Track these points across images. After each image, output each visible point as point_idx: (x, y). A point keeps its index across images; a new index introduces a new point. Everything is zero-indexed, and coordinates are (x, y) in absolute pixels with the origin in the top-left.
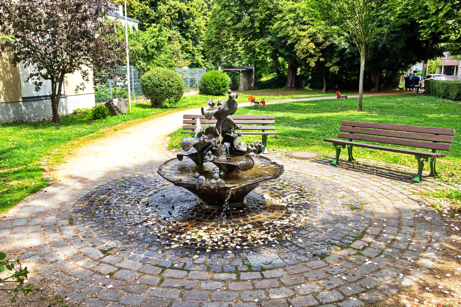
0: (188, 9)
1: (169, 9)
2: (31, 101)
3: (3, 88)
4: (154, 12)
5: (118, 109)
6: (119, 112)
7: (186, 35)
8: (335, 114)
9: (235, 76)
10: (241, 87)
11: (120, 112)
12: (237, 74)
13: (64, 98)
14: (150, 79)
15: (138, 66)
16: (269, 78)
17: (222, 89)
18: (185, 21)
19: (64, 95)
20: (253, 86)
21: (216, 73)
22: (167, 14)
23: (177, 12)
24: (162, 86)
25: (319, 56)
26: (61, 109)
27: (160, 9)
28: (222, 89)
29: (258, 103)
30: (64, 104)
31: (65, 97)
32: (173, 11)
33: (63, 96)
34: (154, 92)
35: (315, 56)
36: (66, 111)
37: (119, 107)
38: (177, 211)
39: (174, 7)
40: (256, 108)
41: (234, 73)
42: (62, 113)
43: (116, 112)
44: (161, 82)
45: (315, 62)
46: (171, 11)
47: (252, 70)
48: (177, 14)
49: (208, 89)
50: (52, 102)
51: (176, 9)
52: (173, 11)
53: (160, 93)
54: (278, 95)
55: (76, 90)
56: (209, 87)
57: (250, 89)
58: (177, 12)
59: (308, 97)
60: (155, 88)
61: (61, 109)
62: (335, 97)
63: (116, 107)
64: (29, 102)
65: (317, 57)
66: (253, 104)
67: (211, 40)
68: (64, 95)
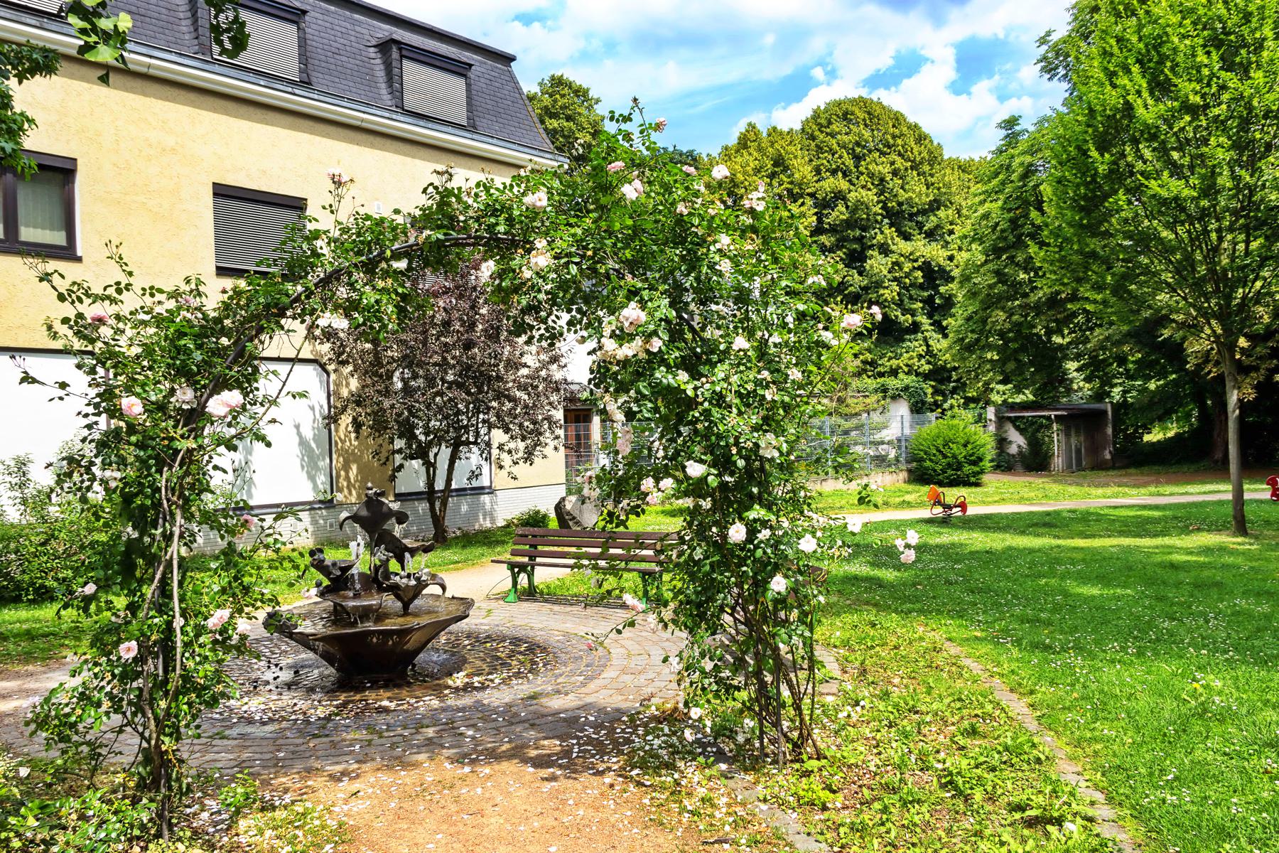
0: (951, 258)
1: (895, 263)
4: (856, 276)
7: (944, 323)
8: (1159, 541)
9: (1038, 430)
10: (1058, 462)
12: (1041, 426)
16: (1170, 434)
17: (967, 469)
18: (942, 289)
20: (1108, 457)
21: (951, 428)
22: (889, 276)
23: (919, 268)
25: (1267, 369)
27: (872, 267)
28: (967, 469)
29: (950, 508)
30: (488, 506)
32: (907, 267)
35: (1256, 369)
36: (493, 520)
38: (1011, 841)
39: (910, 257)
40: (945, 522)
41: (1033, 423)
43: (571, 523)
45: (1256, 387)
46: (901, 269)
47: (1105, 412)
48: (919, 274)
49: (927, 468)
51: (916, 261)
52: (907, 267)
54: (1145, 485)
56: (928, 463)
57: (1080, 468)
58: (919, 268)
59: (1210, 492)
63: (568, 513)
65: (1263, 372)
66: (938, 510)
67: (963, 339)
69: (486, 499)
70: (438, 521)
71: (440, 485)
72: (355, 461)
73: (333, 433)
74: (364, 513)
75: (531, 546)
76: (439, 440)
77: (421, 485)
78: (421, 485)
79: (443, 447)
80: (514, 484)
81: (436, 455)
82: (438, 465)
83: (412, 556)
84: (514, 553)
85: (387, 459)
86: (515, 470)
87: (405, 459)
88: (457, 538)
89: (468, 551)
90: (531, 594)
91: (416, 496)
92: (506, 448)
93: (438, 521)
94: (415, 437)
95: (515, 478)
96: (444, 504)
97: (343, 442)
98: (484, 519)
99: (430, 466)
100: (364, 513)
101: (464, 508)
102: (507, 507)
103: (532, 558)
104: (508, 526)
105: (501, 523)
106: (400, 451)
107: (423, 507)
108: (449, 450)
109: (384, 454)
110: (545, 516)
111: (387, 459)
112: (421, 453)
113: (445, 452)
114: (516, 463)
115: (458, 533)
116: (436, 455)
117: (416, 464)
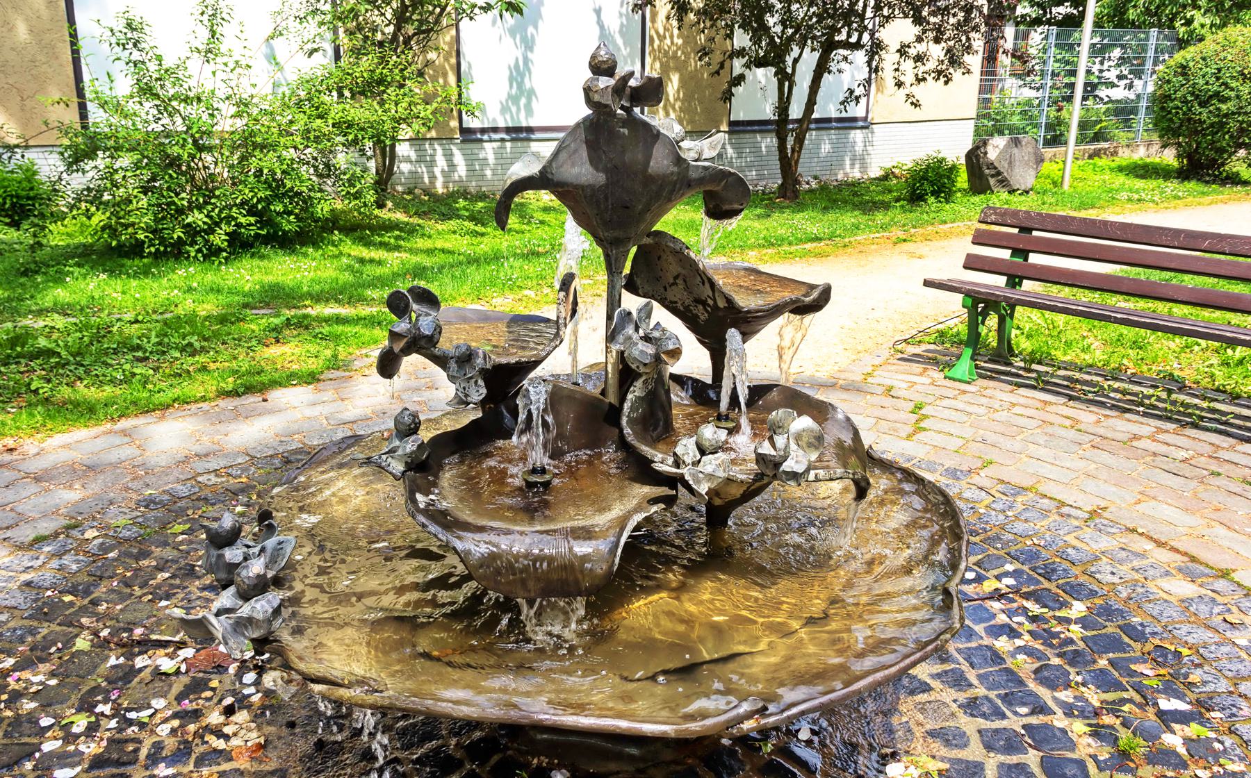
2: (755, 132)
3: (678, 91)
5: (999, 173)
6: (1001, 182)
11: (1004, 183)
13: (862, 128)
14: (1184, 74)
15: (1183, 29)
19: (865, 119)
24: (1224, 100)
26: (848, 162)
30: (859, 148)
31: (867, 128)
33: (861, 124)
34: (1189, 120)
36: (864, 168)
37: (1003, 166)
42: (846, 174)
43: (992, 181)
44: (1226, 85)
50: (779, 138)
53: (1212, 125)
55: (842, 103)
60: (1197, 108)
61: (848, 162)
62: (546, 551)
63: (991, 165)
64: (747, 136)
68: (865, 119)
69: (857, 136)
70: (788, 165)
71: (796, 111)
72: (677, 69)
73: (648, 24)
74: (581, 171)
75: (1016, 252)
76: (802, 34)
77: (768, 111)
78: (768, 111)
79: (807, 50)
80: (916, 114)
81: (796, 61)
82: (797, 78)
83: (746, 336)
84: (972, 263)
85: (722, 65)
86: (919, 91)
87: (747, 66)
88: (811, 191)
89: (831, 216)
90: (999, 360)
91: (759, 126)
92: (912, 52)
93: (788, 165)
94: (765, 28)
95: (916, 105)
96: (800, 140)
97: (662, 38)
98: (852, 165)
99: (785, 78)
100: (581, 171)
101: (826, 148)
102: (891, 148)
103: (1014, 280)
104: (885, 178)
105: (875, 172)
106: (741, 53)
107: (768, 143)
108: (817, 55)
109: (717, 57)
110: (953, 168)
111: (722, 65)
112: (774, 57)
113: (810, 59)
114: (920, 80)
115: (814, 185)
116: (796, 61)
117: (764, 76)
